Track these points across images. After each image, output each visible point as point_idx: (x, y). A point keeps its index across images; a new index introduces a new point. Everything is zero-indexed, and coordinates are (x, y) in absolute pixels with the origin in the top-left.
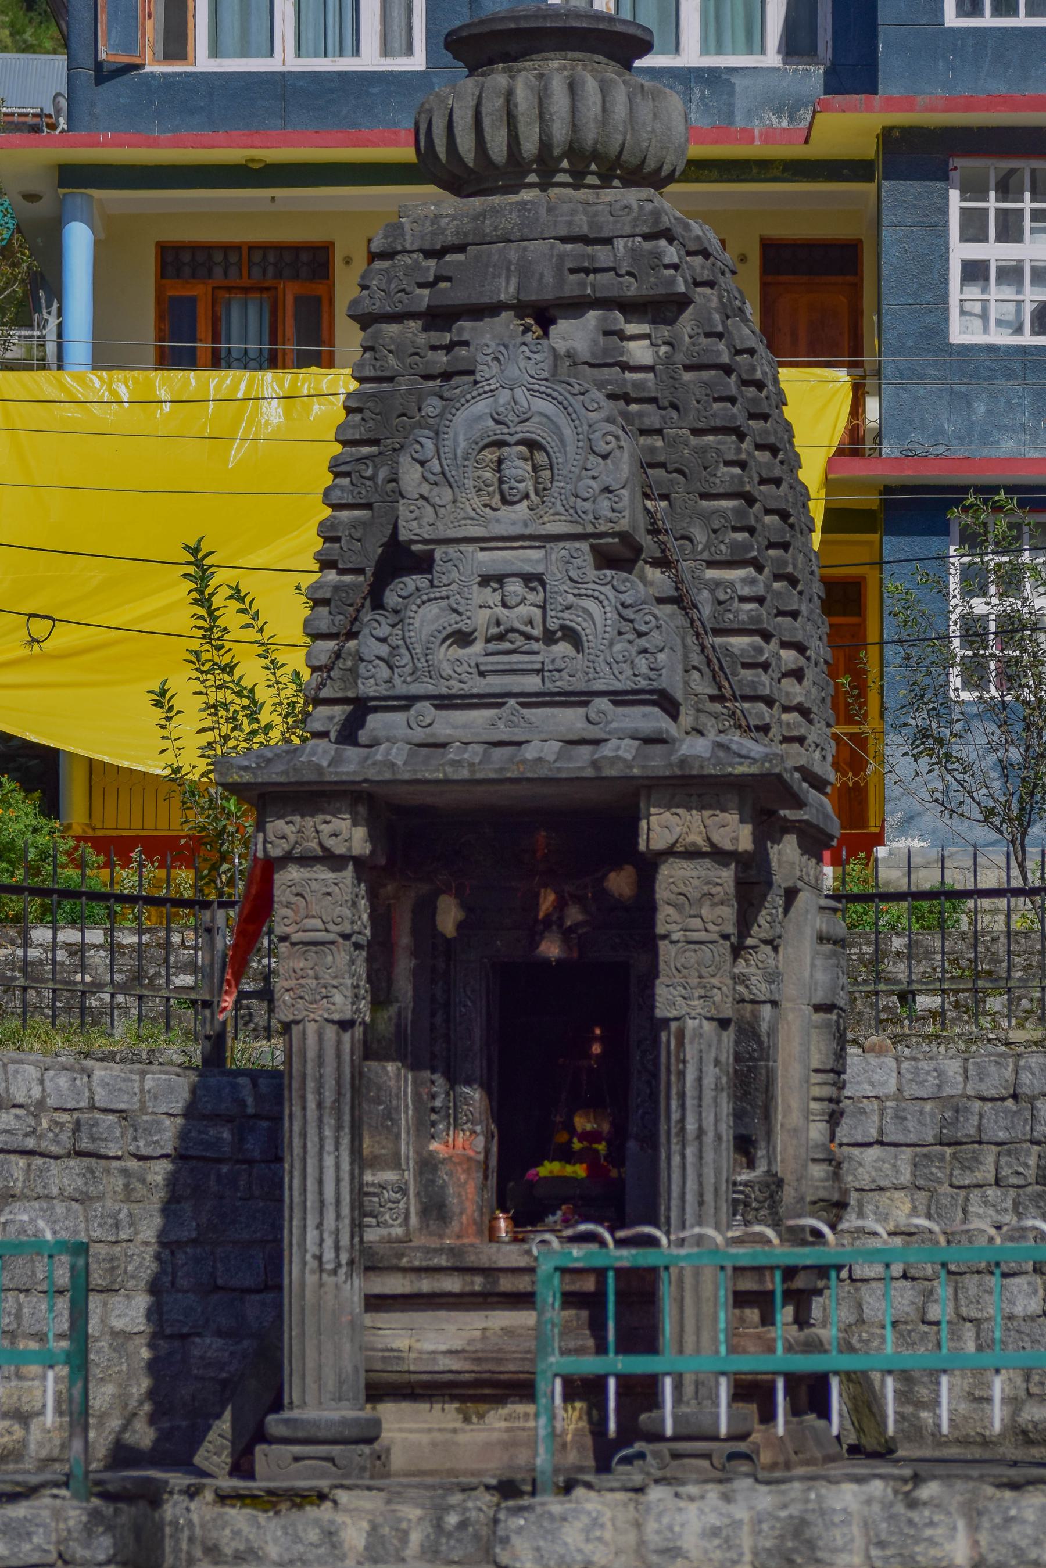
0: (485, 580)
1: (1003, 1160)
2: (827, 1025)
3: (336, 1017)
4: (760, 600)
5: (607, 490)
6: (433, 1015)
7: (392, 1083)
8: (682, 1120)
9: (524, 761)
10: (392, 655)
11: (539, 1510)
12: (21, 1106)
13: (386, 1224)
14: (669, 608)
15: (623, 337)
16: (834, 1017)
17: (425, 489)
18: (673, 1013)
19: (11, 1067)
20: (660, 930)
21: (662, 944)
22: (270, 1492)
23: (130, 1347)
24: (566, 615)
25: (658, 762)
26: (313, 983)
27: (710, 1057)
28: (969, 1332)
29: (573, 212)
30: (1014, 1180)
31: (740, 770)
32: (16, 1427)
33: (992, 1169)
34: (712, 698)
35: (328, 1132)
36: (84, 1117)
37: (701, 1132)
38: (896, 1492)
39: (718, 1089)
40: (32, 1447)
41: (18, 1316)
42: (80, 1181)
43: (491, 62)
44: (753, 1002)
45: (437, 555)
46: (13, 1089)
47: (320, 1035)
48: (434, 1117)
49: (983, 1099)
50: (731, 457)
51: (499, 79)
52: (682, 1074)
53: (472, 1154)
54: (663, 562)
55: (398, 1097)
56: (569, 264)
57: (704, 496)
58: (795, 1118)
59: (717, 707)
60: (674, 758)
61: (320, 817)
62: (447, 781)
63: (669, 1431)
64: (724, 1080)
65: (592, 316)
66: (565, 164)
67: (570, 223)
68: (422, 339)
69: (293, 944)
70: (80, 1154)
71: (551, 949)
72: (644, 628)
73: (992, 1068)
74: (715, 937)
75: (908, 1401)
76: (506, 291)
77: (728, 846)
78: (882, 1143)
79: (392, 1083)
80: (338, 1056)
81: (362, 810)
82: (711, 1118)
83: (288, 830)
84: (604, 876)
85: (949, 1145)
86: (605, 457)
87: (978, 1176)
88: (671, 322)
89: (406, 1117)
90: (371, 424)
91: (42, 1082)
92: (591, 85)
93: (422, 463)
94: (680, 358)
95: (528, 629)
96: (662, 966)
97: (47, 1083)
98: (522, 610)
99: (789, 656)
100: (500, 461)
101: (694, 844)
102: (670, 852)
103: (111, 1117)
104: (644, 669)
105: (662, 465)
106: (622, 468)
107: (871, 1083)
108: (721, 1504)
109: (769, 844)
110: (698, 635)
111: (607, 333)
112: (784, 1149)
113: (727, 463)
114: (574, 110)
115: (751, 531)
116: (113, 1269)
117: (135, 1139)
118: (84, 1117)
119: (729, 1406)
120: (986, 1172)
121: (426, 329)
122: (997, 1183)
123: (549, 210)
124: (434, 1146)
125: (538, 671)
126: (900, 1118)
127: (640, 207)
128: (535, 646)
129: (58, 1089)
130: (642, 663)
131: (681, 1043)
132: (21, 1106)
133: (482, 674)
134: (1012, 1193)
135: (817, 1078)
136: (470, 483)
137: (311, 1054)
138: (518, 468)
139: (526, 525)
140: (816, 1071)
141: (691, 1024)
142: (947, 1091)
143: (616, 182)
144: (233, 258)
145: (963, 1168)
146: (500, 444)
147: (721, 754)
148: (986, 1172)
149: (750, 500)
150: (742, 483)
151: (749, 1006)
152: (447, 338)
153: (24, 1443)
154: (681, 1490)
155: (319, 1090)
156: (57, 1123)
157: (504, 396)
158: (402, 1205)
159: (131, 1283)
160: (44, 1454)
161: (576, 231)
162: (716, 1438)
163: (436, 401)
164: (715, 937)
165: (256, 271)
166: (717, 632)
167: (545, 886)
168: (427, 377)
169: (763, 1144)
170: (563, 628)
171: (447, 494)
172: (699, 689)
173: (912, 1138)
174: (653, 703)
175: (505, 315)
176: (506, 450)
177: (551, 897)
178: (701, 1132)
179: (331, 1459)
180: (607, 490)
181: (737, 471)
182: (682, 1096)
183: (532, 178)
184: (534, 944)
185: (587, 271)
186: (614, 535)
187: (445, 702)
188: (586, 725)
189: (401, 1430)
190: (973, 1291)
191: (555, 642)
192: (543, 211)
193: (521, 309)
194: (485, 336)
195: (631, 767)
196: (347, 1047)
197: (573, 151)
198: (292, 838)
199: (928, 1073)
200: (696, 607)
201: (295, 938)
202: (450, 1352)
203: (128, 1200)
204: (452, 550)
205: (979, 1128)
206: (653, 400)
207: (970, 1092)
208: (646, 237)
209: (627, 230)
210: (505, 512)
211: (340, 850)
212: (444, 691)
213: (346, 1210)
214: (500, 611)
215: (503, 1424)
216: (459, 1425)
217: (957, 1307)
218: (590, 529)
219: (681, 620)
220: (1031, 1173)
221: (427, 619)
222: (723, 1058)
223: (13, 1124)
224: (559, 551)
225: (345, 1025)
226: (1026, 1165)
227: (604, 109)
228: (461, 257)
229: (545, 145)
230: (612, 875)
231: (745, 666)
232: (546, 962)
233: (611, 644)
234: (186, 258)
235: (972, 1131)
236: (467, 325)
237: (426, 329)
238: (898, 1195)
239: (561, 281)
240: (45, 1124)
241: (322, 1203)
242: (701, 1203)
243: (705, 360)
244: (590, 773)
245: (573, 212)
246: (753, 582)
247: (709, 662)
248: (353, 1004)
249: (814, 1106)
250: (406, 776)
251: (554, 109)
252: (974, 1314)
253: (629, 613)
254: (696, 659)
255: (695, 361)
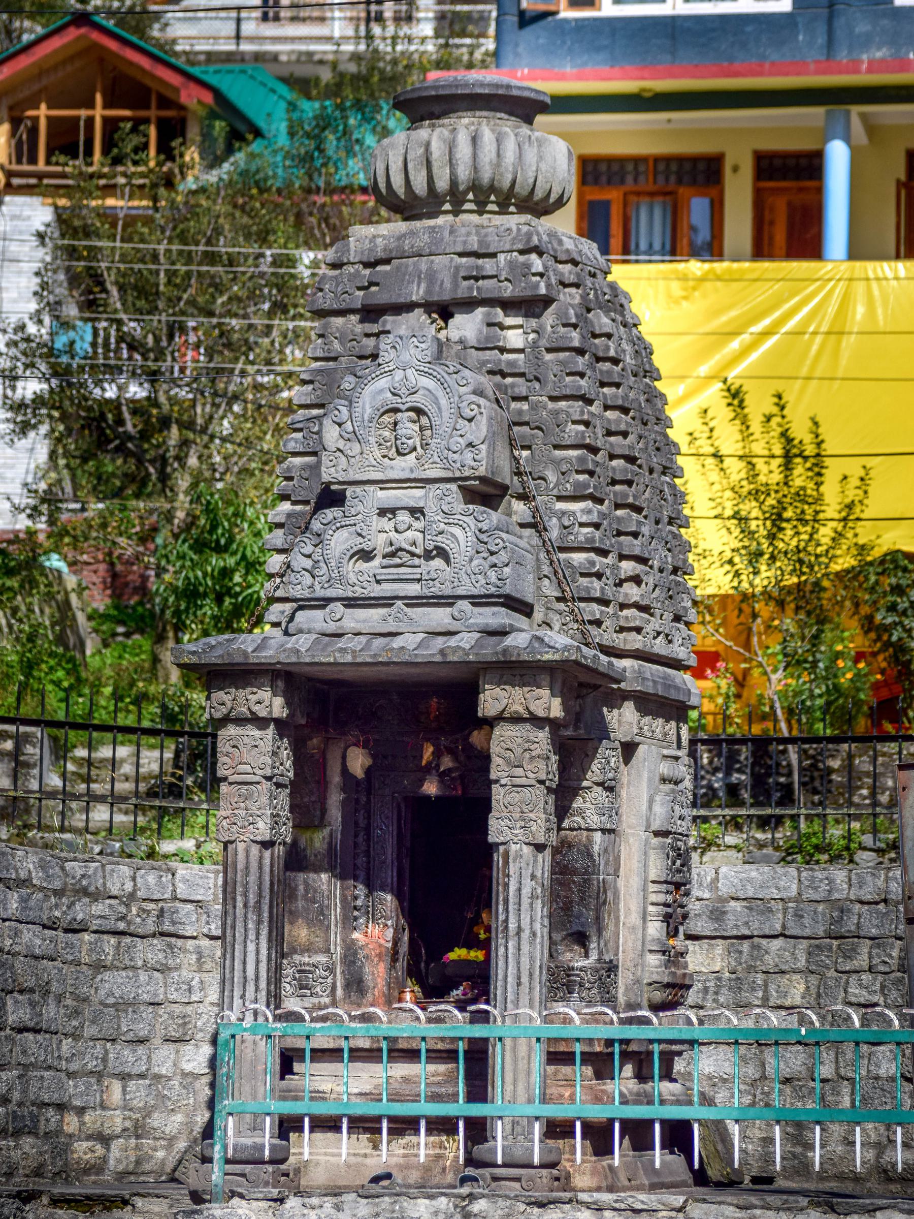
0: (382, 512)
1: (875, 951)
2: (663, 847)
3: (259, 838)
4: (597, 526)
5: (470, 445)
6: (356, 836)
7: (324, 887)
8: (506, 921)
9: (392, 649)
10: (314, 567)
11: (205, 1213)
12: (115, 897)
13: (317, 995)
14: (527, 532)
15: (502, 327)
16: (669, 840)
17: (341, 444)
18: (502, 839)
19: (108, 867)
20: (493, 776)
21: (495, 788)
22: (88, 1198)
23: (197, 1085)
24: (439, 538)
25: (490, 650)
26: (243, 813)
27: (526, 874)
28: (846, 1089)
29: (468, 234)
30: (882, 968)
31: (546, 657)
32: (98, 1147)
33: (866, 958)
34: (558, 599)
35: (251, 925)
36: (167, 906)
37: (519, 930)
38: (456, 1206)
39: (533, 897)
40: (112, 1162)
41: (105, 1060)
42: (161, 955)
43: (422, 119)
44: (588, 830)
45: (348, 493)
46: (109, 884)
47: (247, 853)
48: (356, 913)
49: (862, 902)
50: (577, 417)
51: (423, 133)
52: (506, 885)
53: (382, 941)
54: (523, 497)
55: (329, 898)
56: (462, 274)
57: (556, 447)
58: (634, 918)
59: (561, 606)
60: (499, 649)
61: (249, 689)
62: (336, 664)
63: (536, 1161)
64: (539, 890)
65: (480, 311)
66: (471, 196)
67: (465, 242)
68: (359, 329)
69: (231, 784)
70: (162, 934)
71: (431, 788)
72: (494, 549)
73: (869, 878)
74: (533, 782)
75: (799, 1143)
76: (417, 293)
77: (541, 713)
78: (786, 936)
79: (324, 887)
80: (260, 867)
81: (280, 684)
82: (528, 920)
83: (227, 698)
84: (470, 733)
85: (836, 938)
86: (470, 420)
87: (856, 964)
88: (538, 316)
89: (336, 913)
90: (319, 392)
91: (134, 879)
92: (488, 136)
93: (340, 425)
94: (544, 343)
95: (413, 549)
96: (494, 803)
97: (139, 880)
98: (409, 534)
99: (628, 567)
100: (396, 424)
101: (516, 712)
102: (500, 718)
103: (189, 906)
104: (493, 579)
105: (527, 424)
106: (480, 430)
107: (778, 888)
108: (333, 1211)
109: (605, 710)
110: (548, 552)
111: (489, 325)
112: (625, 943)
113: (574, 422)
114: (475, 156)
115: (591, 473)
116: (185, 1024)
117: (208, 923)
118: (167, 906)
119: (541, 1141)
120: (862, 961)
121: (362, 321)
122: (870, 970)
123: (451, 232)
124: (356, 935)
125: (419, 580)
126: (798, 916)
127: (519, 230)
128: (416, 561)
129: (147, 884)
130: (493, 575)
131: (506, 863)
132: (115, 897)
133: (378, 582)
134: (880, 978)
135: (652, 888)
136: (373, 440)
137: (240, 866)
138: (408, 428)
139: (412, 471)
140: (653, 882)
141: (514, 848)
142: (836, 896)
143: (512, 209)
144: (642, 168)
145: (846, 957)
146: (396, 410)
147: (537, 645)
148: (862, 961)
149: (594, 450)
150: (584, 438)
151: (585, 833)
152: (375, 328)
153: (105, 1159)
154: (307, 1200)
155: (245, 895)
156: (144, 910)
157: (399, 375)
158: (329, 980)
159: (199, 1036)
160: (121, 1168)
161: (469, 248)
162: (530, 1166)
163: (352, 379)
164: (533, 782)
165: (661, 179)
166: (562, 549)
167: (428, 740)
168: (361, 357)
169: (594, 939)
170: (437, 548)
171: (356, 448)
172: (548, 593)
173: (807, 932)
174: (502, 605)
175: (418, 311)
176: (399, 415)
177: (431, 749)
178: (519, 930)
179: (243, 1175)
180: (470, 445)
181: (582, 428)
182: (506, 902)
183: (447, 207)
184: (421, 782)
185: (477, 279)
186: (475, 478)
187: (351, 603)
188: (451, 620)
189: (326, 1154)
190: (849, 1055)
191: (433, 558)
192: (446, 233)
193: (429, 307)
194: (400, 325)
195: (468, 655)
196: (267, 861)
197: (475, 186)
198: (229, 705)
199: (821, 881)
200: (546, 530)
201: (232, 779)
202: (361, 1094)
203: (200, 970)
204: (358, 490)
205: (858, 926)
206: (522, 375)
207: (852, 897)
208: (522, 252)
209: (507, 247)
210: (400, 462)
211: (263, 714)
212: (350, 594)
213: (263, 985)
214: (393, 534)
215: (402, 1151)
216: (369, 1151)
217: (837, 1068)
218: (458, 474)
219: (536, 541)
220: (894, 963)
221: (340, 542)
222: (539, 874)
223: (107, 912)
224: (435, 490)
225: (266, 845)
226: (890, 956)
227: (498, 155)
228: (387, 268)
229: (454, 183)
230: (475, 733)
231: (582, 575)
232: (428, 797)
233: (471, 560)
234: (603, 167)
235: (853, 928)
236: (389, 318)
237: (362, 321)
238: (796, 977)
239: (456, 285)
240: (134, 911)
241: (245, 978)
242: (519, 984)
243: (561, 344)
244: (438, 658)
245: (468, 234)
246: (589, 512)
247: (555, 572)
248: (272, 829)
249: (651, 909)
250: (307, 660)
251: (458, 156)
252: (850, 1074)
253: (483, 537)
254: (546, 570)
255: (554, 345)
